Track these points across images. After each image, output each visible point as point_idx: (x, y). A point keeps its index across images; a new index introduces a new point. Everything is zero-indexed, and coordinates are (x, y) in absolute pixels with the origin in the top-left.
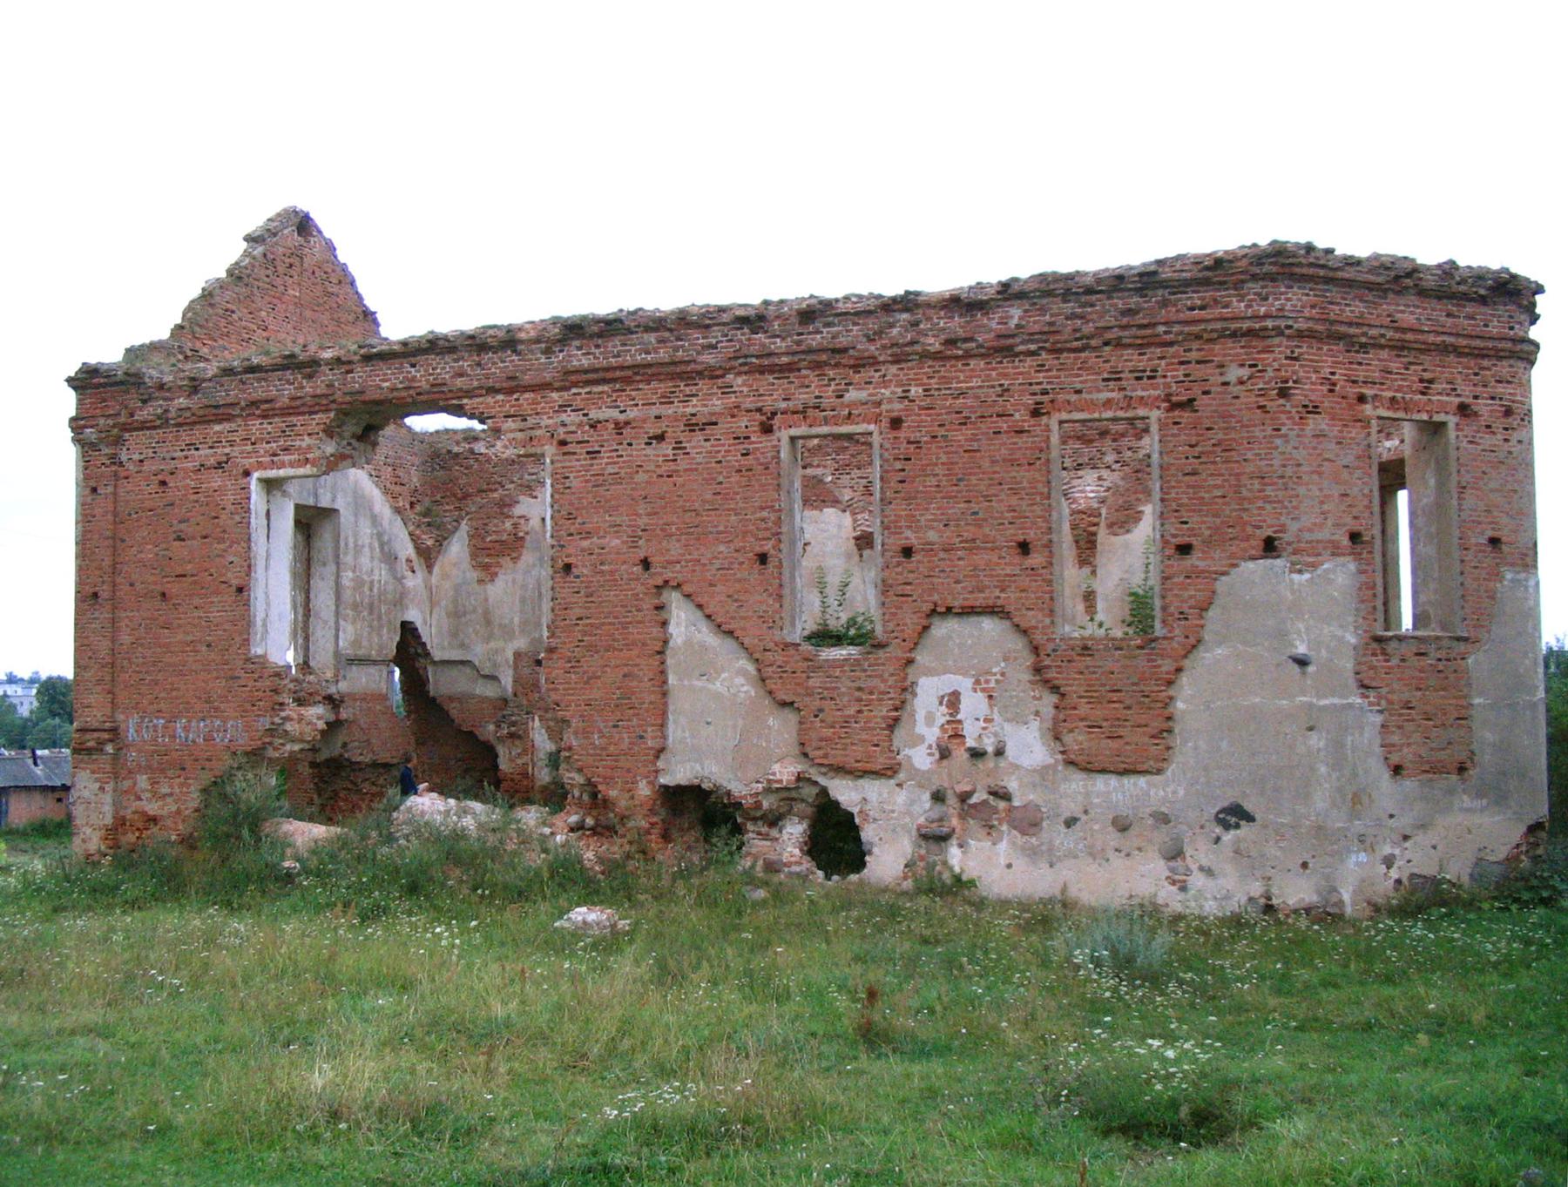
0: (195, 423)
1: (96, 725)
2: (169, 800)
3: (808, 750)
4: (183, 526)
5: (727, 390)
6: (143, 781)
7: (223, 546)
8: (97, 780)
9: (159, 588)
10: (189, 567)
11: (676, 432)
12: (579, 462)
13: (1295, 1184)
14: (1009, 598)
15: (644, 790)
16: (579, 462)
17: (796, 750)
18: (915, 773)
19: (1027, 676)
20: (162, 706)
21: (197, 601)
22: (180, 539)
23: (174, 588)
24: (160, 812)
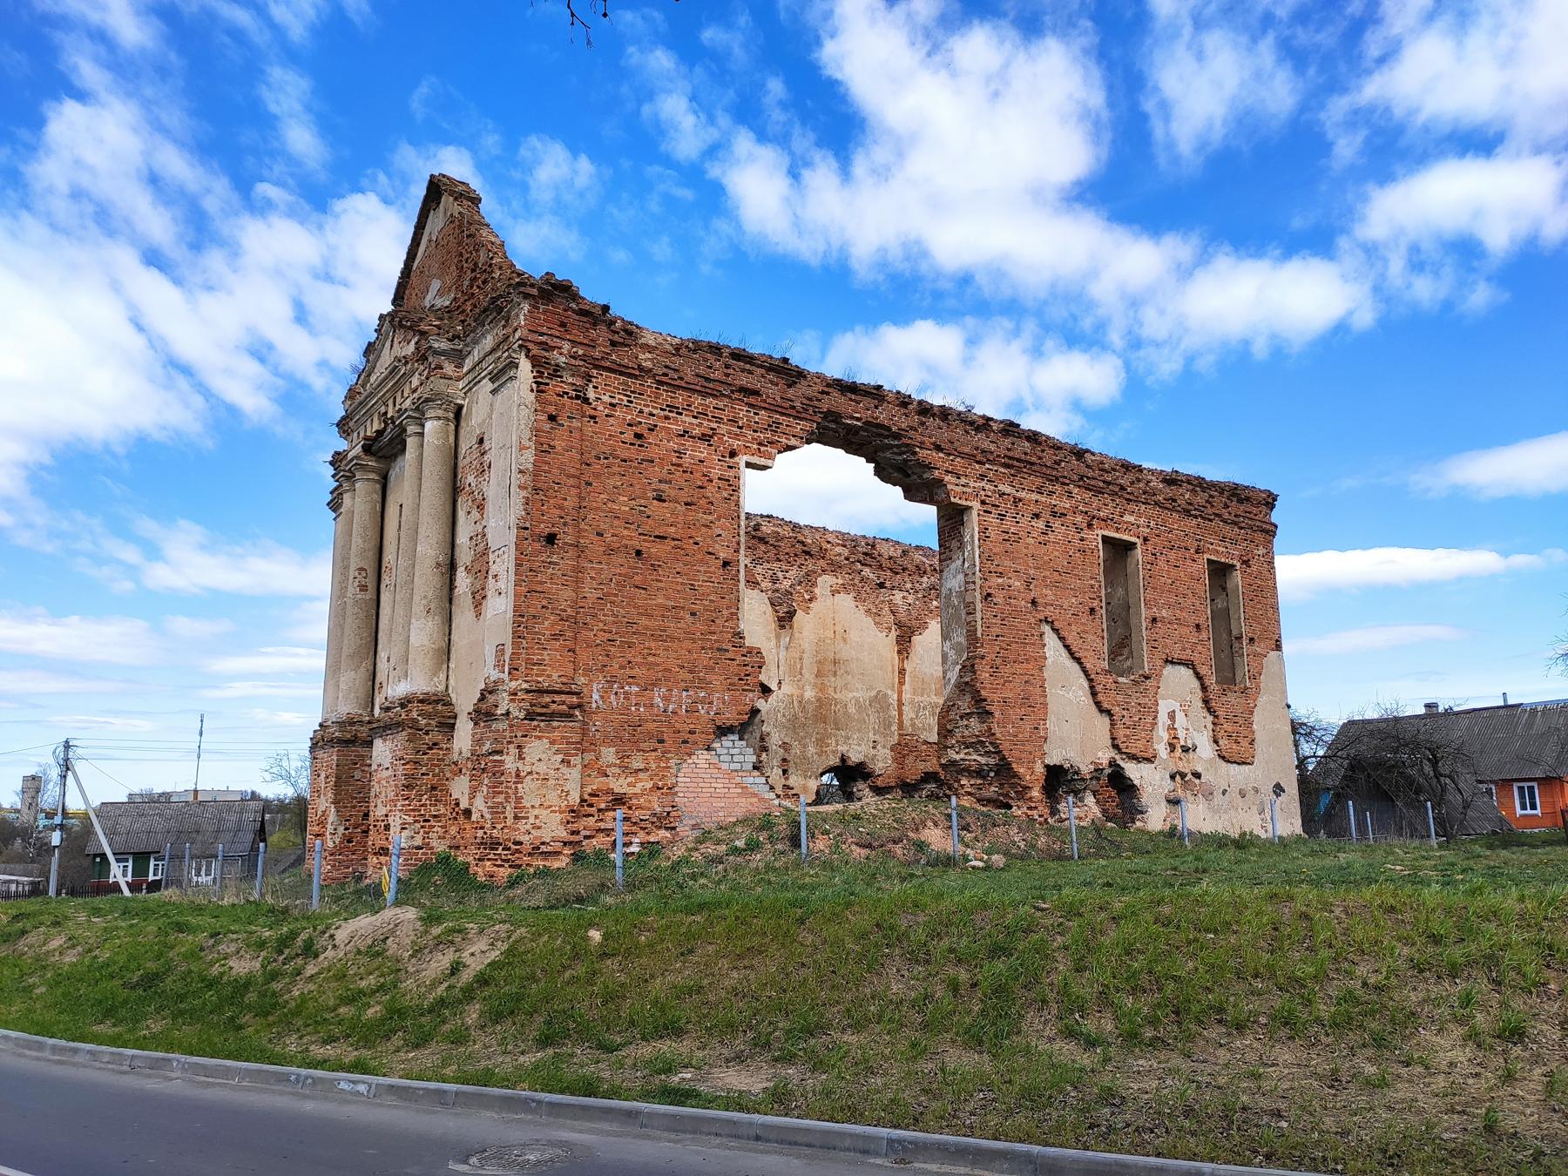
0: (679, 387)
1: (557, 687)
2: (641, 775)
3: (1118, 742)
4: (663, 486)
5: (1070, 495)
6: (609, 754)
7: (710, 518)
8: (558, 752)
9: (636, 544)
10: (673, 529)
11: (1046, 515)
12: (992, 519)
13: (1083, 3)
14: (1196, 658)
15: (1039, 769)
16: (992, 519)
17: (1109, 742)
18: (292, 161)
19: (1200, 704)
20: (636, 671)
21: (679, 567)
22: (660, 499)
23: (655, 549)
24: (631, 791)
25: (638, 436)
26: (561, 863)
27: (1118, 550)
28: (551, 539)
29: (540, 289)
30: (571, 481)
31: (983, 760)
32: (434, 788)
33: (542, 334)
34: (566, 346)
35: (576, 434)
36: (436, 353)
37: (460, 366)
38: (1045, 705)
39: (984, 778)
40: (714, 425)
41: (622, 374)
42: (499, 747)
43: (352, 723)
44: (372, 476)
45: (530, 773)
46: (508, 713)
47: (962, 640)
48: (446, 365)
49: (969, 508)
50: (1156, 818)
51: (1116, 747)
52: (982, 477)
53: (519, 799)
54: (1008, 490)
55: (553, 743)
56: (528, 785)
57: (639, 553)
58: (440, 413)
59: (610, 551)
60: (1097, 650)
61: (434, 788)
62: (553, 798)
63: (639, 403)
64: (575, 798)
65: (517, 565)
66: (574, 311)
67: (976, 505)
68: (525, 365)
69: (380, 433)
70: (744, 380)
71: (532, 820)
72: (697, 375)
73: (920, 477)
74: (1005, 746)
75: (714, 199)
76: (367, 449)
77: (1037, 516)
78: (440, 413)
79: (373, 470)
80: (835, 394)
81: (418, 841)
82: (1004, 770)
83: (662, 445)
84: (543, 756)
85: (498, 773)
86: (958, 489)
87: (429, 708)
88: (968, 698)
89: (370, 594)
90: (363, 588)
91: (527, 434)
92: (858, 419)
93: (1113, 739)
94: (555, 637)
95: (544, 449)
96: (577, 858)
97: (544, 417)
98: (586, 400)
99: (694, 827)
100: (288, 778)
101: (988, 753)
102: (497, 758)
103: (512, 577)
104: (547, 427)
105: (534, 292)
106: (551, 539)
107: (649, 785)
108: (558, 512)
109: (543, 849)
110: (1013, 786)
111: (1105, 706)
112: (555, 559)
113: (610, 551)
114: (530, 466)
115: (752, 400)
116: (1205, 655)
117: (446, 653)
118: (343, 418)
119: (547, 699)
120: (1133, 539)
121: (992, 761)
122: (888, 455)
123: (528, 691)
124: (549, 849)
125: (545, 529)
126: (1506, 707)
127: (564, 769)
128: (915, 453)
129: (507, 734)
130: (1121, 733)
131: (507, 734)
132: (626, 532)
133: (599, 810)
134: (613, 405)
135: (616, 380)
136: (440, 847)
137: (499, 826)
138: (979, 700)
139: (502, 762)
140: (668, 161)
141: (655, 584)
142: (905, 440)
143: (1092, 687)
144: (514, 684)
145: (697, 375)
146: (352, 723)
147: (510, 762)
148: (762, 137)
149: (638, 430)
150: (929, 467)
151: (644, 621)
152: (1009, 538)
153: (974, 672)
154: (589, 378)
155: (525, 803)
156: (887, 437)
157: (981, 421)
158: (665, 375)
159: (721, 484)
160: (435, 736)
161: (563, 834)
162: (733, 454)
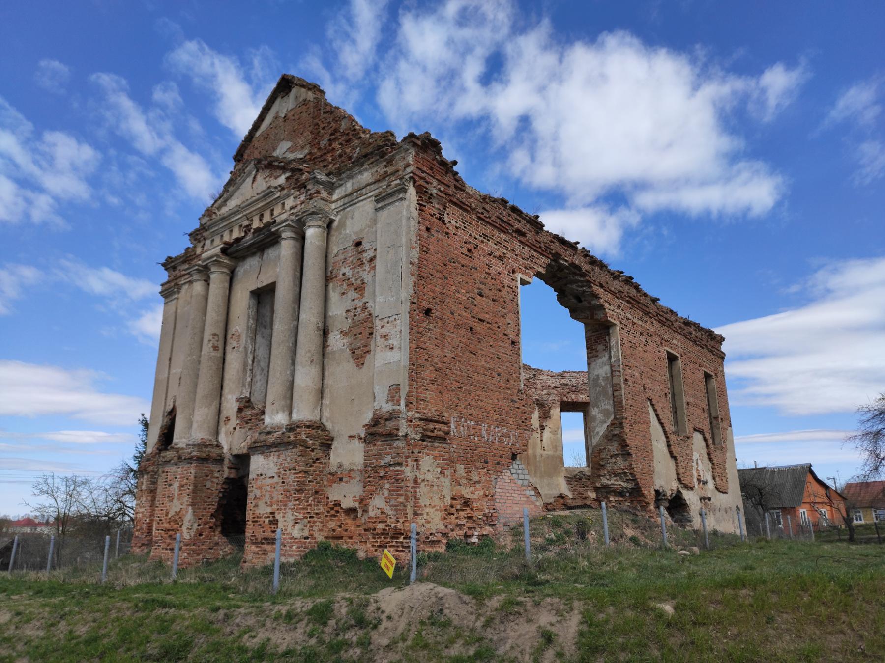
2: (478, 486)
7: (505, 311)
10: (487, 316)
17: (675, 477)
20: (472, 411)
23: (479, 327)
25: (469, 251)
26: (442, 549)
27: (672, 359)
28: (428, 312)
29: (423, 142)
30: (438, 275)
31: (624, 485)
32: (316, 492)
33: (423, 172)
34: (435, 183)
35: (440, 243)
36: (318, 182)
37: (331, 194)
38: (652, 450)
39: (623, 496)
40: (505, 251)
41: (461, 208)
42: (400, 460)
43: (206, 446)
44: (225, 270)
45: (423, 480)
46: (406, 435)
47: (610, 407)
48: (322, 191)
49: (615, 325)
50: (696, 523)
51: (679, 480)
52: (619, 307)
53: (417, 500)
54: (630, 317)
55: (435, 458)
56: (422, 490)
57: (471, 329)
58: (320, 223)
59: (458, 326)
60: (667, 416)
61: (316, 492)
62: (436, 501)
63: (470, 229)
64: (448, 501)
65: (411, 329)
66: (437, 161)
67: (617, 322)
68: (412, 191)
69: (238, 240)
70: (517, 226)
71: (425, 516)
72: (498, 217)
73: (589, 303)
74: (638, 476)
75: (169, 178)
76: (224, 251)
77: (641, 334)
78: (320, 223)
79: (226, 266)
80: (557, 243)
81: (306, 533)
82: (636, 493)
83: (480, 260)
84: (430, 469)
85: (398, 479)
86: (611, 312)
87: (313, 432)
88: (616, 444)
89: (219, 354)
90: (215, 348)
91: (414, 238)
92: (566, 261)
93: (678, 474)
94: (433, 382)
95: (424, 250)
96: (449, 546)
97: (424, 228)
98: (443, 221)
99: (505, 524)
100: (51, 493)
101: (628, 481)
102: (398, 468)
103: (408, 337)
104: (425, 234)
105: (419, 143)
106: (428, 312)
107: (482, 493)
108: (432, 294)
109: (432, 538)
110: (640, 502)
111: (675, 454)
112: (431, 326)
113: (458, 326)
114: (417, 261)
115: (521, 238)
116: (706, 427)
117: (321, 393)
118: (197, 230)
119: (431, 426)
120: (677, 355)
121: (630, 486)
122: (574, 287)
123: (421, 420)
124: (435, 539)
125: (425, 305)
126: (756, 469)
127: (442, 479)
128: (591, 287)
129: (405, 450)
130: (681, 471)
131: (405, 450)
132: (465, 314)
133: (457, 510)
134: (457, 228)
135: (458, 212)
136: (320, 537)
137: (401, 520)
138: (624, 445)
139: (401, 471)
140: (138, 153)
141: (480, 351)
142: (588, 278)
143: (668, 442)
144: (410, 414)
145: (498, 217)
146: (206, 446)
147: (408, 472)
148: (191, 148)
149: (469, 246)
150: (597, 297)
151: (475, 376)
152: (633, 347)
153: (623, 428)
154: (445, 207)
155: (422, 503)
156: (577, 275)
157: (617, 274)
158: (482, 213)
159: (509, 289)
160: (318, 453)
161: (442, 527)
162: (514, 272)
